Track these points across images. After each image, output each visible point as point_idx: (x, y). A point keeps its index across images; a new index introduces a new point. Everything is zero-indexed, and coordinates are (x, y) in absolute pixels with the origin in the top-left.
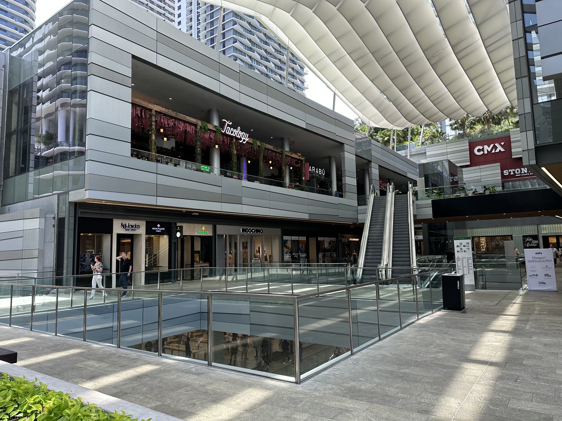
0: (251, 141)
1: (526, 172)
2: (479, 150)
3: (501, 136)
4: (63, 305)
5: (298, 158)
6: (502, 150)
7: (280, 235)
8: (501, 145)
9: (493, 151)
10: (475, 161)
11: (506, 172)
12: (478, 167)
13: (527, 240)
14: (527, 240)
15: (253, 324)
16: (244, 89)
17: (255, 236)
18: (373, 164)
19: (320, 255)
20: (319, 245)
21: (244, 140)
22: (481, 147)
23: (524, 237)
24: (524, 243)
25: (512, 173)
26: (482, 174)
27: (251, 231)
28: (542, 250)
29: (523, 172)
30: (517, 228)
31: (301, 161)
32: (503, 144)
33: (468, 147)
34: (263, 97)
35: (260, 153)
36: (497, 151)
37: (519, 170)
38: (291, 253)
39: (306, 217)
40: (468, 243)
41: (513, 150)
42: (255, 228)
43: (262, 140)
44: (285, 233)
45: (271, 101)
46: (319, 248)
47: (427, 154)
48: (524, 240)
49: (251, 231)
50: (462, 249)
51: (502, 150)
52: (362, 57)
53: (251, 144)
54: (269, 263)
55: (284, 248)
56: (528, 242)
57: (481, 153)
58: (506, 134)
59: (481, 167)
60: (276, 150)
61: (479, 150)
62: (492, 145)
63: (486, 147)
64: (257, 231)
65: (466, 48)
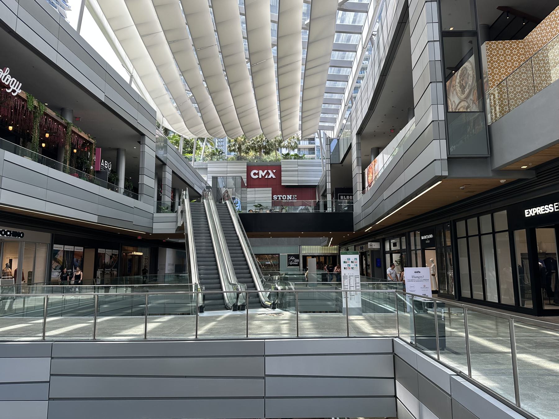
0: (24, 96)
2: (255, 174)
3: (273, 164)
5: (87, 138)
6: (274, 177)
7: (49, 241)
8: (273, 172)
9: (266, 177)
10: (251, 183)
12: (253, 189)
13: (291, 258)
14: (291, 258)
15: (54, 399)
16: (23, 14)
17: (7, 241)
18: (167, 168)
19: (99, 273)
20: (98, 258)
21: (14, 91)
22: (257, 172)
23: (289, 255)
24: (288, 261)
25: (280, 199)
26: (257, 196)
27: (6, 233)
28: (420, 269)
31: (91, 143)
32: (274, 171)
33: (246, 169)
34: (53, 40)
35: (35, 118)
36: (270, 177)
38: (62, 269)
39: (93, 219)
40: (356, 259)
41: (283, 178)
42: (13, 230)
43: (41, 101)
44: (56, 240)
45: (62, 48)
46: (98, 262)
47: (209, 169)
48: (289, 259)
49: (6, 233)
50: (349, 265)
51: (274, 177)
52: (178, 41)
53: (24, 100)
54: (26, 285)
55: (53, 262)
56: (291, 260)
57: (257, 177)
58: (277, 163)
59: (256, 189)
60: (59, 120)
61: (255, 174)
62: (266, 171)
63: (261, 172)
64: (15, 234)
65: (287, 65)
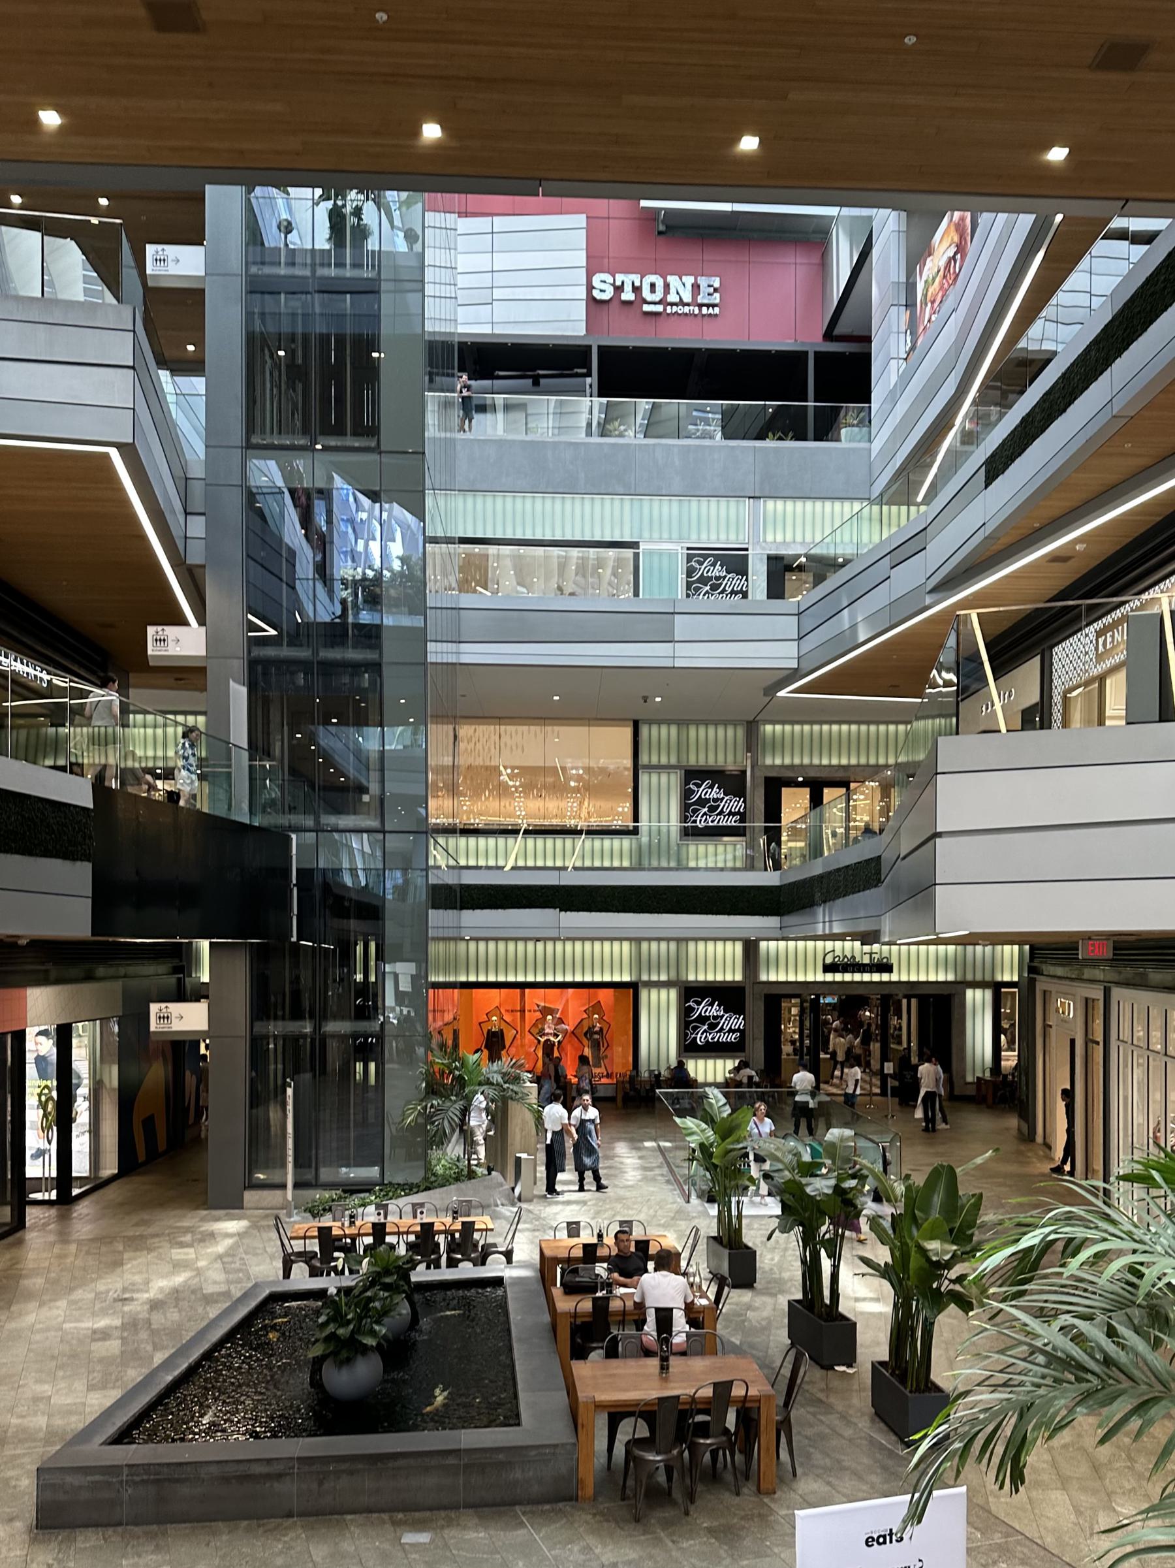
1: (687, 298)
4: (269, 1226)
11: (603, 287)
26: (502, 261)
29: (672, 298)
30: (665, 509)
37: (659, 283)
